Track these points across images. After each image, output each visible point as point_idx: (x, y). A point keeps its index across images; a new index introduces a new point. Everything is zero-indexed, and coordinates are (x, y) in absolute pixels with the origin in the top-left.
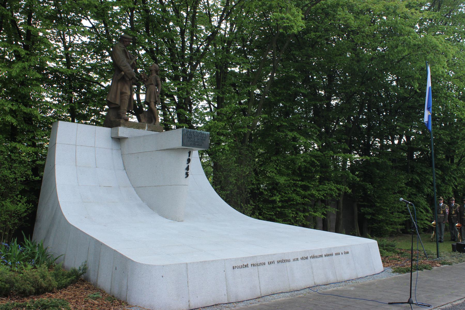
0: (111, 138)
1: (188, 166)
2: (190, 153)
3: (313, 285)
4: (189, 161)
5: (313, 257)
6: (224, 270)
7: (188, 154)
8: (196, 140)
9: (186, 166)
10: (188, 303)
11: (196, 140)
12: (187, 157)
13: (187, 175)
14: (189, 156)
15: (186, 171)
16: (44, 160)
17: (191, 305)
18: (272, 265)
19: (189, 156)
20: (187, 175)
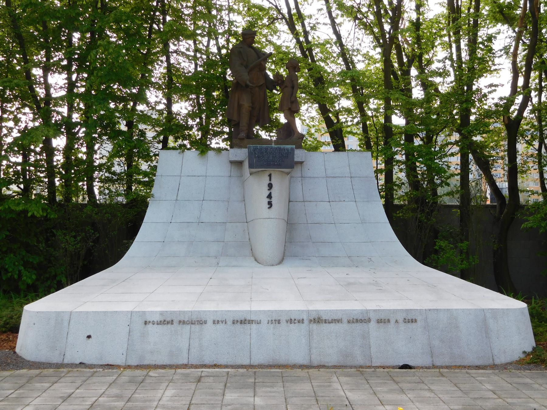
0: (229, 164)
1: (271, 193)
2: (270, 176)
3: (305, 362)
4: (270, 186)
5: (291, 321)
6: (129, 324)
7: (268, 178)
8: (271, 158)
9: (267, 193)
10: (430, 349)
11: (271, 158)
12: (268, 182)
13: (270, 204)
14: (270, 180)
15: (268, 200)
16: (149, 184)
17: (313, 357)
18: (221, 326)
19: (270, 180)
20: (270, 204)
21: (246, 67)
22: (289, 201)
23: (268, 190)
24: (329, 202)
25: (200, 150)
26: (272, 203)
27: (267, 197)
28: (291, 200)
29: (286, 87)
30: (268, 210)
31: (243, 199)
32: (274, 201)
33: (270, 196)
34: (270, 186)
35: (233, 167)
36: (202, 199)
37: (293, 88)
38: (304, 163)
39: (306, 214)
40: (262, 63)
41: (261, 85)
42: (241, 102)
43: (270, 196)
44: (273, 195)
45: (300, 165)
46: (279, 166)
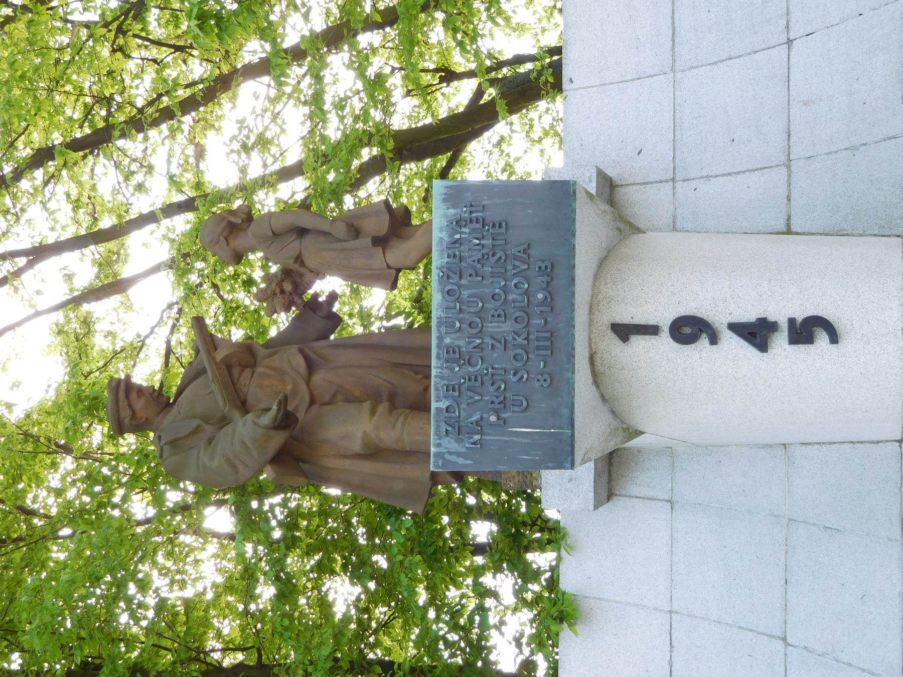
0: (615, 501)
1: (736, 328)
4: (690, 329)
7: (639, 342)
11: (506, 327)
12: (665, 342)
13: (804, 331)
14: (651, 330)
19: (651, 330)
20: (804, 331)
21: (224, 421)
22: (789, 232)
23: (714, 339)
24: (790, 42)
25: (554, 628)
26: (800, 317)
27: (763, 347)
28: (781, 225)
29: (299, 260)
30: (848, 343)
31: (780, 451)
32: (783, 308)
33: (757, 333)
34: (690, 329)
35: (633, 490)
36: (780, 644)
37: (302, 232)
38: (610, 172)
39: (853, 148)
40: (220, 355)
41: (307, 359)
42: (357, 446)
43: (757, 333)
44: (749, 315)
45: (620, 192)
46: (556, 273)
